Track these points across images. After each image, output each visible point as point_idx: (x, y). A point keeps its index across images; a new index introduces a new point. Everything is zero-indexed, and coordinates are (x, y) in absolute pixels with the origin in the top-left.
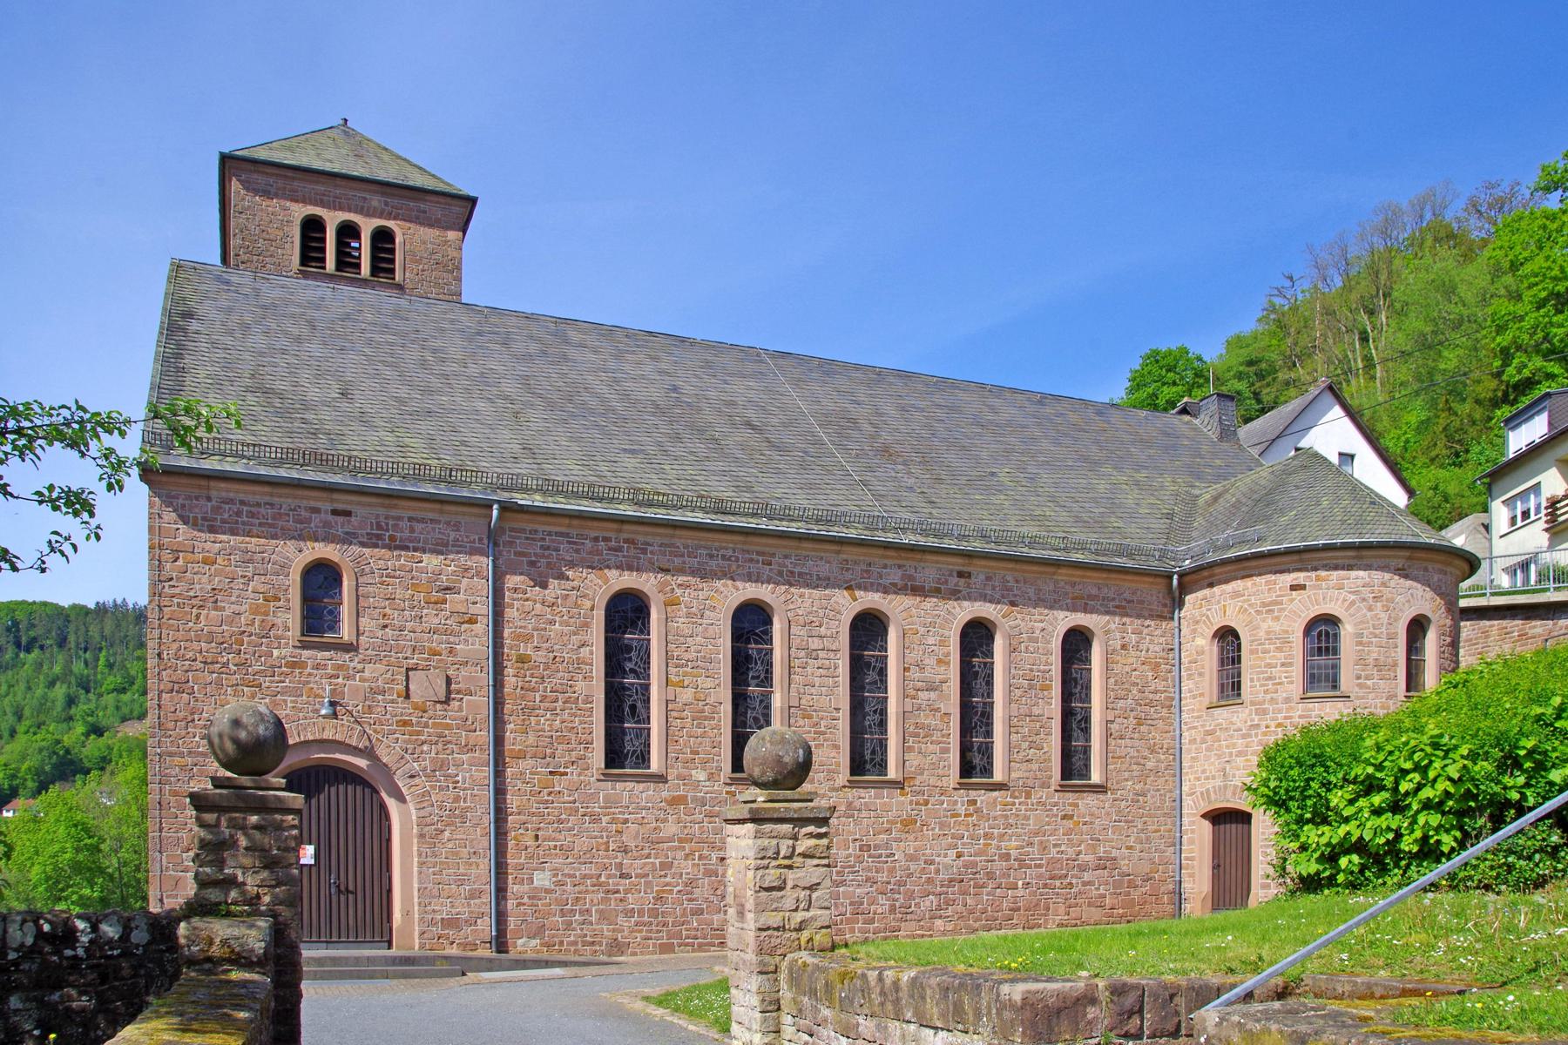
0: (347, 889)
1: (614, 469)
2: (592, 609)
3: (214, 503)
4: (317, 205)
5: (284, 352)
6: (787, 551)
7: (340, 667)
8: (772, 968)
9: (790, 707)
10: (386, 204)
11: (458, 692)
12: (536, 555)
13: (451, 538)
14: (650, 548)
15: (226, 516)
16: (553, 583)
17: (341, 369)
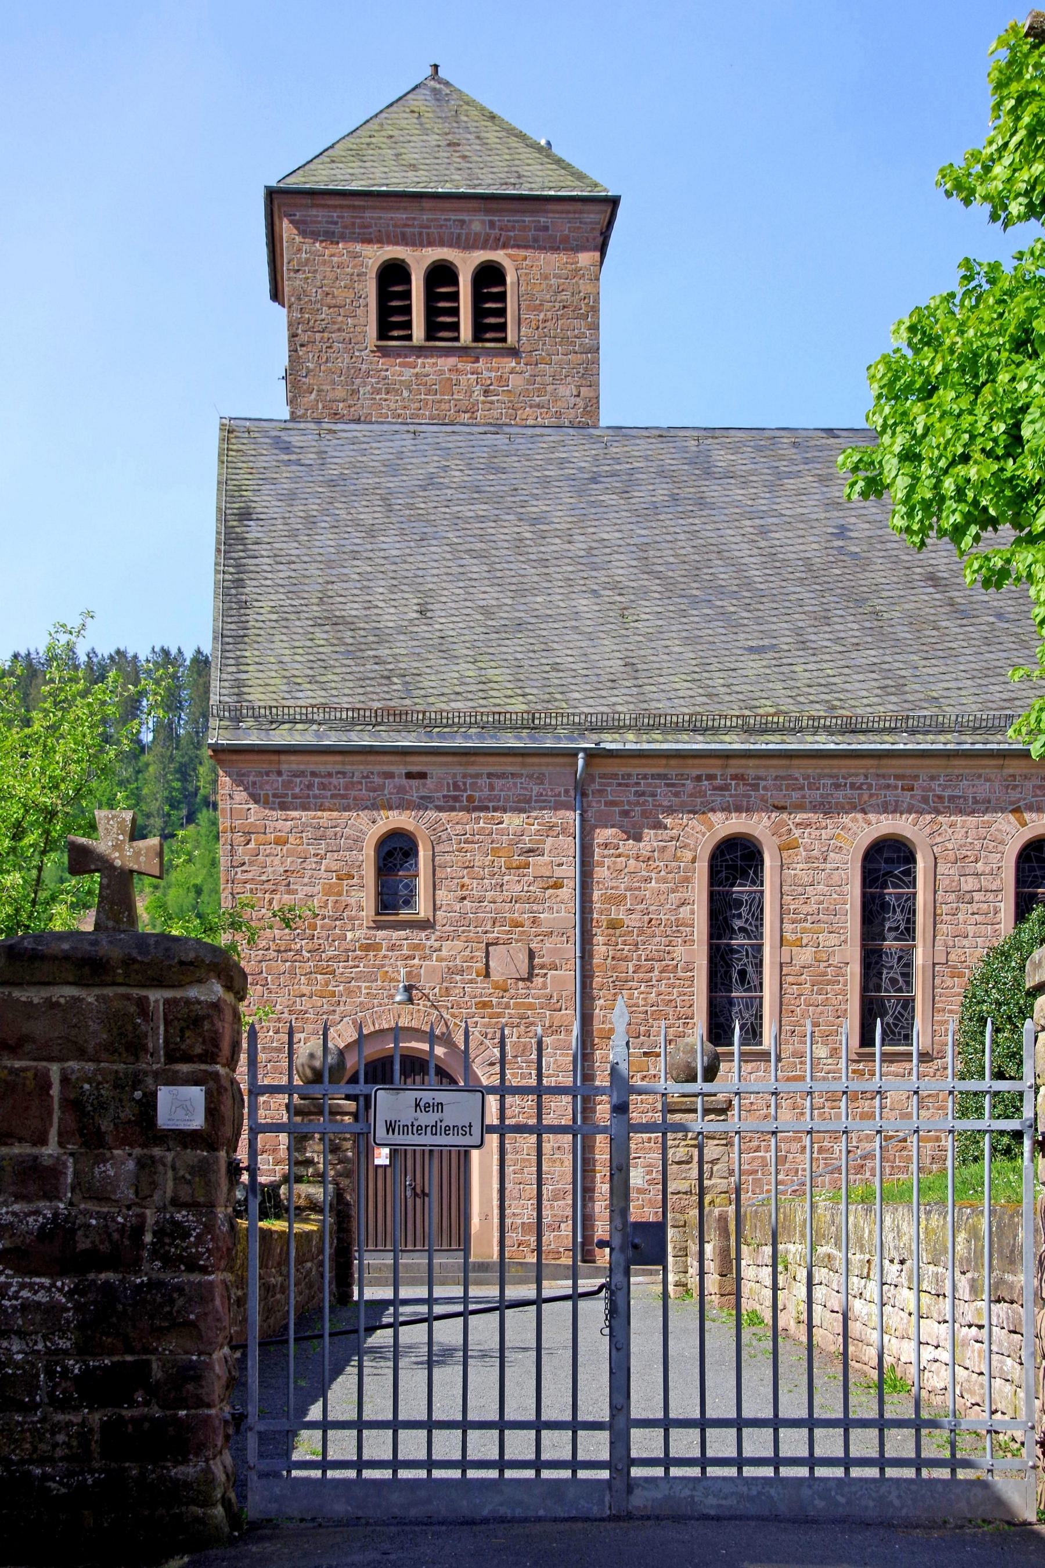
0: (423, 1191)
1: (731, 681)
2: (694, 861)
3: (285, 777)
4: (397, 244)
5: (355, 555)
6: (934, 771)
7: (416, 947)
8: (682, 1223)
9: (934, 964)
10: (492, 224)
11: (542, 967)
12: (629, 803)
13: (534, 793)
14: (762, 783)
15: (297, 790)
16: (649, 833)
17: (420, 573)
